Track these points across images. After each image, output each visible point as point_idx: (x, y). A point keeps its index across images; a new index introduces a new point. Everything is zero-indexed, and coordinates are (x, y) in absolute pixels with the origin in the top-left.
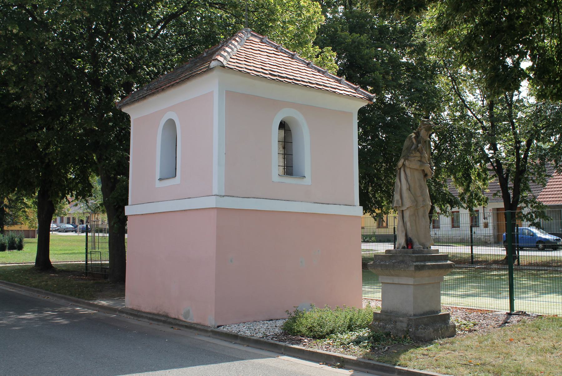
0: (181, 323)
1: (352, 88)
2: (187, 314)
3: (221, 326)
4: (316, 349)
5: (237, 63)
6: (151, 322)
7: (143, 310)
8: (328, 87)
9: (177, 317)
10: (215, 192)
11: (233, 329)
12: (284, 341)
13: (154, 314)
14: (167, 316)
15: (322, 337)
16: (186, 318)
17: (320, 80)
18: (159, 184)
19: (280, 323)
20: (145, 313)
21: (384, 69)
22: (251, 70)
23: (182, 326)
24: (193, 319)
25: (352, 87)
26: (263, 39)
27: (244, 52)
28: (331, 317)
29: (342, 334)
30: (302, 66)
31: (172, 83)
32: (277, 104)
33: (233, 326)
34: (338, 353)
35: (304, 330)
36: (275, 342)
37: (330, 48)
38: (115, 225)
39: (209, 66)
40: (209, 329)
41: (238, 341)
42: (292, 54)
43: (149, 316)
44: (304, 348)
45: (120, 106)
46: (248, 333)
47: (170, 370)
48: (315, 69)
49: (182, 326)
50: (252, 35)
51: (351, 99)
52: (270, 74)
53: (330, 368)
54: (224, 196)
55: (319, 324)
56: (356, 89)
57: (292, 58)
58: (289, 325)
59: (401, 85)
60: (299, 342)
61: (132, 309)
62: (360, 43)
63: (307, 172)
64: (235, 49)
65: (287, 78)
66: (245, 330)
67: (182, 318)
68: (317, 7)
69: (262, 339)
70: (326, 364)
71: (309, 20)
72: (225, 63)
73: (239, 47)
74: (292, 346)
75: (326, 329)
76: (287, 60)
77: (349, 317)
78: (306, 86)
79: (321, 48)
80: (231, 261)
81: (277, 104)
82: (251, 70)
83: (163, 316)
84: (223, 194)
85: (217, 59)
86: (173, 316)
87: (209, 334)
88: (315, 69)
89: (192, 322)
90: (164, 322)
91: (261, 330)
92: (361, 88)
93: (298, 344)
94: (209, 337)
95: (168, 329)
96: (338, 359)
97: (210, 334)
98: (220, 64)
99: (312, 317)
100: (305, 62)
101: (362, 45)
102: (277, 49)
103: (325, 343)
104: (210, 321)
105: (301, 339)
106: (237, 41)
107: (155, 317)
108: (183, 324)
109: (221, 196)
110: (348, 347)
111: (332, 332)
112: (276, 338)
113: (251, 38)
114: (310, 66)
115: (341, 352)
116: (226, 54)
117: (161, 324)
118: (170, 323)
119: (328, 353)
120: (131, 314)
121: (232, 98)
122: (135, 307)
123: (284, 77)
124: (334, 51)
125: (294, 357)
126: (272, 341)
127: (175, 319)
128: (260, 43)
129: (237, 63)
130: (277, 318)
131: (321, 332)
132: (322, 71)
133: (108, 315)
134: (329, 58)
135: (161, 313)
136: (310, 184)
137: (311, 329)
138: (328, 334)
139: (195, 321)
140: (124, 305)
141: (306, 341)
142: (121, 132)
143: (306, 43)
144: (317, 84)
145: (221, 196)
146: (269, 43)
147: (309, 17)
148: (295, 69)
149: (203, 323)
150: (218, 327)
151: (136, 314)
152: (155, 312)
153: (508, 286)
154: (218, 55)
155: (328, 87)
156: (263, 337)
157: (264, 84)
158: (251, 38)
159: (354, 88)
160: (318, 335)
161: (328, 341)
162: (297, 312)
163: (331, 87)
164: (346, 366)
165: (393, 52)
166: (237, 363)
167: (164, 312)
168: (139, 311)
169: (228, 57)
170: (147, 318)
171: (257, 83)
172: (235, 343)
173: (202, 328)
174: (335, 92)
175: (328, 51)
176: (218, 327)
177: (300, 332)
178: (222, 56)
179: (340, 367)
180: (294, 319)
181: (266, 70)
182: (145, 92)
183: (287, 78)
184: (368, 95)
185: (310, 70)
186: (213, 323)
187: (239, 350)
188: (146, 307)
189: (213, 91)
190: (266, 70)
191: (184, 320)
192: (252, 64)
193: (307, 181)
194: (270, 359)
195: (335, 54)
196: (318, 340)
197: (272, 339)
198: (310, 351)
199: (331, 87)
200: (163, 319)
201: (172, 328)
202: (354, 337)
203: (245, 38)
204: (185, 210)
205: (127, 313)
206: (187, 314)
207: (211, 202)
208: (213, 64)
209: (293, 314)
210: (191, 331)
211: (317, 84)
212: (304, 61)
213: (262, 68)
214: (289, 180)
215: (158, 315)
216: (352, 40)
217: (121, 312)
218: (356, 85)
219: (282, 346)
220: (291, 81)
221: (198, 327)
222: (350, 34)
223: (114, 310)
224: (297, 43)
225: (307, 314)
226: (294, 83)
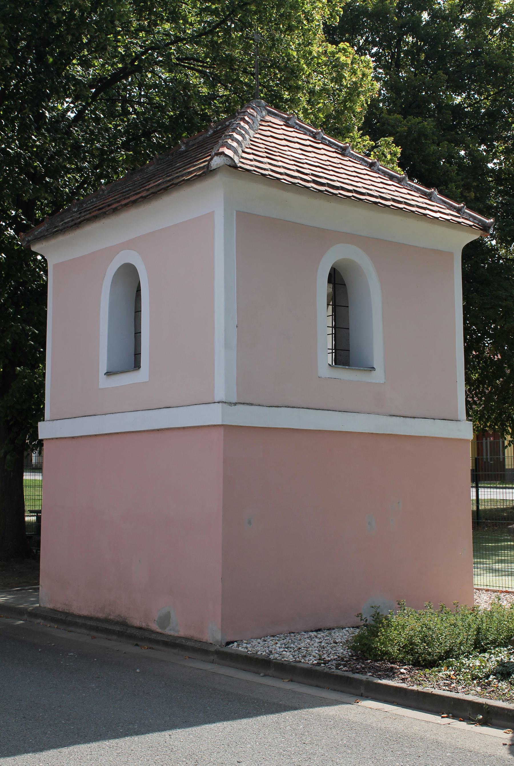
0: (153, 636)
1: (451, 207)
2: (165, 620)
3: (233, 642)
4: (428, 688)
5: (256, 160)
6: (93, 633)
7: (76, 611)
8: (412, 206)
9: (144, 625)
10: (220, 394)
11: (258, 648)
12: (361, 671)
13: (97, 619)
14: (124, 623)
15: (431, 664)
16: (163, 627)
17: (396, 194)
18: (105, 383)
19: (341, 636)
20: (80, 617)
21: (462, 180)
22: (281, 174)
23: (157, 642)
24: (178, 628)
25: (451, 206)
26: (288, 119)
27: (267, 141)
28: (443, 629)
29: (467, 657)
30: (362, 169)
31: (133, 198)
32: (324, 237)
33: (255, 642)
34: (473, 695)
35: (394, 650)
36: (346, 674)
37: (391, 139)
38: (8, 457)
39: (208, 166)
40: (212, 649)
41: (271, 671)
42: (341, 147)
43: (89, 623)
44: (404, 685)
45: (29, 242)
46: (289, 657)
47: (170, 732)
48: (385, 173)
49: (157, 642)
50: (270, 113)
51: (446, 227)
52: (314, 182)
53: (463, 725)
54: (235, 404)
55: (423, 640)
56: (458, 210)
57: (343, 155)
58: (365, 641)
59: (491, 207)
60: (391, 673)
61: (54, 611)
62: (422, 134)
63: (378, 359)
64: (247, 136)
65: (343, 189)
66: (279, 650)
67: (155, 627)
68: (367, 66)
69: (318, 668)
70: (454, 717)
71: (354, 91)
72: (236, 159)
73: (251, 132)
74: (380, 681)
75: (438, 650)
76: (336, 159)
77: (474, 626)
78: (376, 203)
79: (374, 138)
80: (250, 523)
81: (324, 237)
82: (281, 174)
83: (117, 623)
84: (235, 400)
85: (223, 153)
86: (137, 623)
87: (212, 658)
88: (385, 173)
89: (176, 634)
90: (120, 634)
91: (310, 650)
92: (468, 208)
93: (388, 677)
94: (213, 662)
95: (129, 648)
96: (478, 707)
97: (214, 657)
98: (229, 162)
99: (406, 625)
100: (366, 162)
101: (426, 136)
102: (314, 137)
103: (440, 675)
104: (213, 633)
105: (392, 668)
106: (247, 123)
107: (100, 625)
108: (159, 638)
109: (230, 404)
110: (489, 684)
111: (448, 654)
112: (345, 666)
113: (268, 118)
114: (376, 168)
115: (478, 694)
116: (235, 144)
117: (114, 637)
118: (131, 637)
119: (453, 695)
120: (53, 620)
121: (248, 224)
122: (60, 607)
123: (337, 188)
124: (397, 145)
125: (398, 704)
126: (339, 672)
127: (141, 628)
128: (284, 127)
129: (256, 160)
130: (331, 625)
131: (429, 654)
132: (396, 177)
133: (9, 621)
134: (389, 157)
135: (112, 617)
136: (382, 381)
137: (409, 648)
138: (441, 658)
139: (182, 632)
140: (37, 602)
141: (402, 671)
142: (16, 289)
143: (349, 130)
144: (394, 200)
145: (230, 404)
146: (301, 127)
147: (355, 83)
148: (351, 173)
149: (197, 636)
150: (228, 643)
151: (64, 619)
152: (100, 615)
153: (27, 492)
154: (222, 146)
155: (412, 206)
156: (319, 664)
157: (304, 199)
158: (268, 118)
159: (455, 208)
160: (425, 663)
161: (444, 672)
162: (378, 618)
163: (418, 207)
164: (494, 721)
165: (83, 196)
166: (287, 715)
167: (119, 616)
168: (68, 614)
169: (240, 151)
170: (84, 626)
171: (291, 196)
172: (265, 675)
173: (197, 645)
174: (425, 215)
175: (388, 145)
176: (228, 643)
177: (387, 653)
178: (230, 147)
179: (484, 723)
180: (373, 632)
181: (307, 174)
182: (76, 215)
183: (343, 189)
184: (480, 221)
185: (377, 175)
186: (219, 637)
187: (261, 684)
188: (81, 605)
189: (213, 212)
190: (307, 174)
191: (159, 630)
192: (280, 164)
193: (378, 376)
194: (343, 706)
195: (399, 150)
196: (427, 671)
197: (337, 668)
198: (418, 692)
199: (418, 207)
200: (117, 628)
201: (137, 645)
202: (492, 665)
203: (259, 118)
204: (158, 430)
205: (45, 618)
206: (165, 620)
207: (213, 415)
208: (216, 162)
209: (370, 621)
210: (176, 651)
211: (394, 200)
212: (363, 160)
213: (298, 171)
214: (345, 374)
215: (107, 621)
216: (409, 128)
217: (34, 614)
218: (459, 203)
219: (360, 682)
220: (350, 194)
221: (189, 643)
222: (404, 118)
223: (20, 613)
224: (333, 127)
225: (394, 620)
226: (356, 199)
